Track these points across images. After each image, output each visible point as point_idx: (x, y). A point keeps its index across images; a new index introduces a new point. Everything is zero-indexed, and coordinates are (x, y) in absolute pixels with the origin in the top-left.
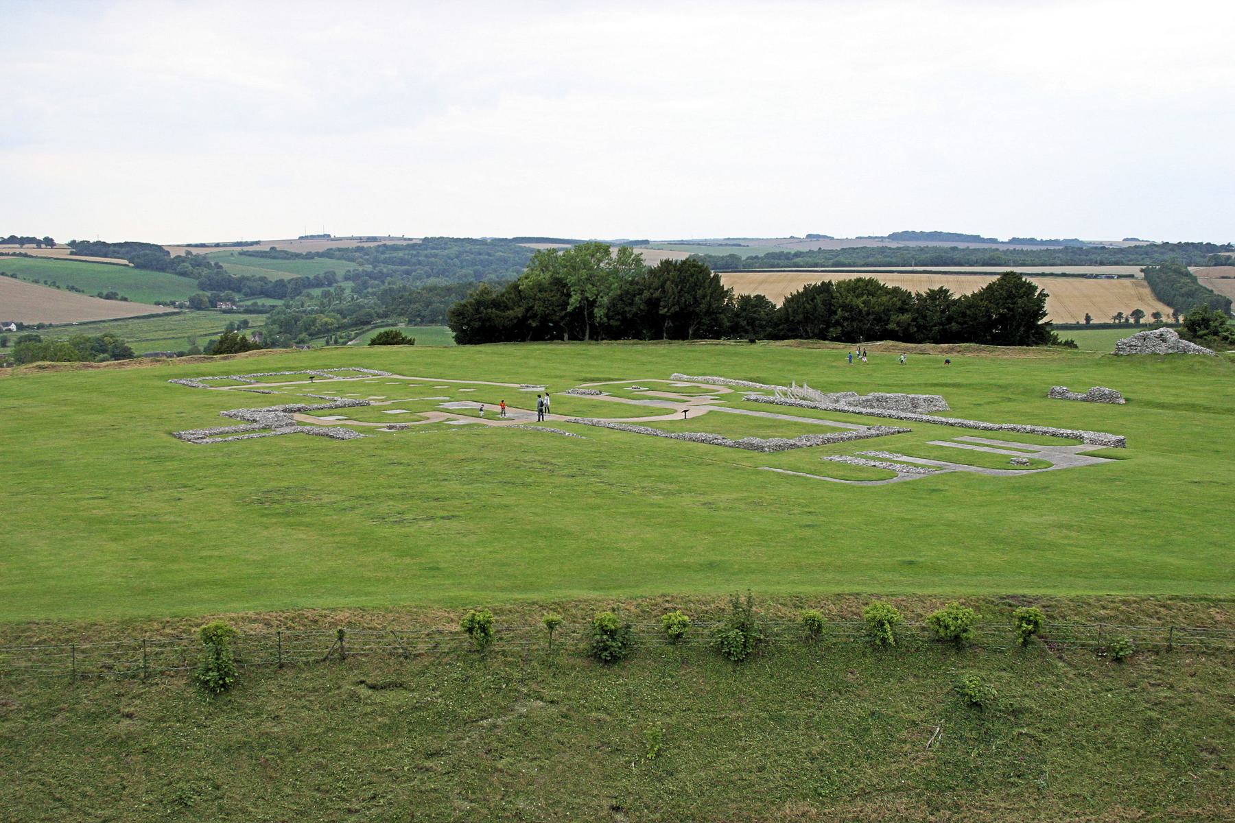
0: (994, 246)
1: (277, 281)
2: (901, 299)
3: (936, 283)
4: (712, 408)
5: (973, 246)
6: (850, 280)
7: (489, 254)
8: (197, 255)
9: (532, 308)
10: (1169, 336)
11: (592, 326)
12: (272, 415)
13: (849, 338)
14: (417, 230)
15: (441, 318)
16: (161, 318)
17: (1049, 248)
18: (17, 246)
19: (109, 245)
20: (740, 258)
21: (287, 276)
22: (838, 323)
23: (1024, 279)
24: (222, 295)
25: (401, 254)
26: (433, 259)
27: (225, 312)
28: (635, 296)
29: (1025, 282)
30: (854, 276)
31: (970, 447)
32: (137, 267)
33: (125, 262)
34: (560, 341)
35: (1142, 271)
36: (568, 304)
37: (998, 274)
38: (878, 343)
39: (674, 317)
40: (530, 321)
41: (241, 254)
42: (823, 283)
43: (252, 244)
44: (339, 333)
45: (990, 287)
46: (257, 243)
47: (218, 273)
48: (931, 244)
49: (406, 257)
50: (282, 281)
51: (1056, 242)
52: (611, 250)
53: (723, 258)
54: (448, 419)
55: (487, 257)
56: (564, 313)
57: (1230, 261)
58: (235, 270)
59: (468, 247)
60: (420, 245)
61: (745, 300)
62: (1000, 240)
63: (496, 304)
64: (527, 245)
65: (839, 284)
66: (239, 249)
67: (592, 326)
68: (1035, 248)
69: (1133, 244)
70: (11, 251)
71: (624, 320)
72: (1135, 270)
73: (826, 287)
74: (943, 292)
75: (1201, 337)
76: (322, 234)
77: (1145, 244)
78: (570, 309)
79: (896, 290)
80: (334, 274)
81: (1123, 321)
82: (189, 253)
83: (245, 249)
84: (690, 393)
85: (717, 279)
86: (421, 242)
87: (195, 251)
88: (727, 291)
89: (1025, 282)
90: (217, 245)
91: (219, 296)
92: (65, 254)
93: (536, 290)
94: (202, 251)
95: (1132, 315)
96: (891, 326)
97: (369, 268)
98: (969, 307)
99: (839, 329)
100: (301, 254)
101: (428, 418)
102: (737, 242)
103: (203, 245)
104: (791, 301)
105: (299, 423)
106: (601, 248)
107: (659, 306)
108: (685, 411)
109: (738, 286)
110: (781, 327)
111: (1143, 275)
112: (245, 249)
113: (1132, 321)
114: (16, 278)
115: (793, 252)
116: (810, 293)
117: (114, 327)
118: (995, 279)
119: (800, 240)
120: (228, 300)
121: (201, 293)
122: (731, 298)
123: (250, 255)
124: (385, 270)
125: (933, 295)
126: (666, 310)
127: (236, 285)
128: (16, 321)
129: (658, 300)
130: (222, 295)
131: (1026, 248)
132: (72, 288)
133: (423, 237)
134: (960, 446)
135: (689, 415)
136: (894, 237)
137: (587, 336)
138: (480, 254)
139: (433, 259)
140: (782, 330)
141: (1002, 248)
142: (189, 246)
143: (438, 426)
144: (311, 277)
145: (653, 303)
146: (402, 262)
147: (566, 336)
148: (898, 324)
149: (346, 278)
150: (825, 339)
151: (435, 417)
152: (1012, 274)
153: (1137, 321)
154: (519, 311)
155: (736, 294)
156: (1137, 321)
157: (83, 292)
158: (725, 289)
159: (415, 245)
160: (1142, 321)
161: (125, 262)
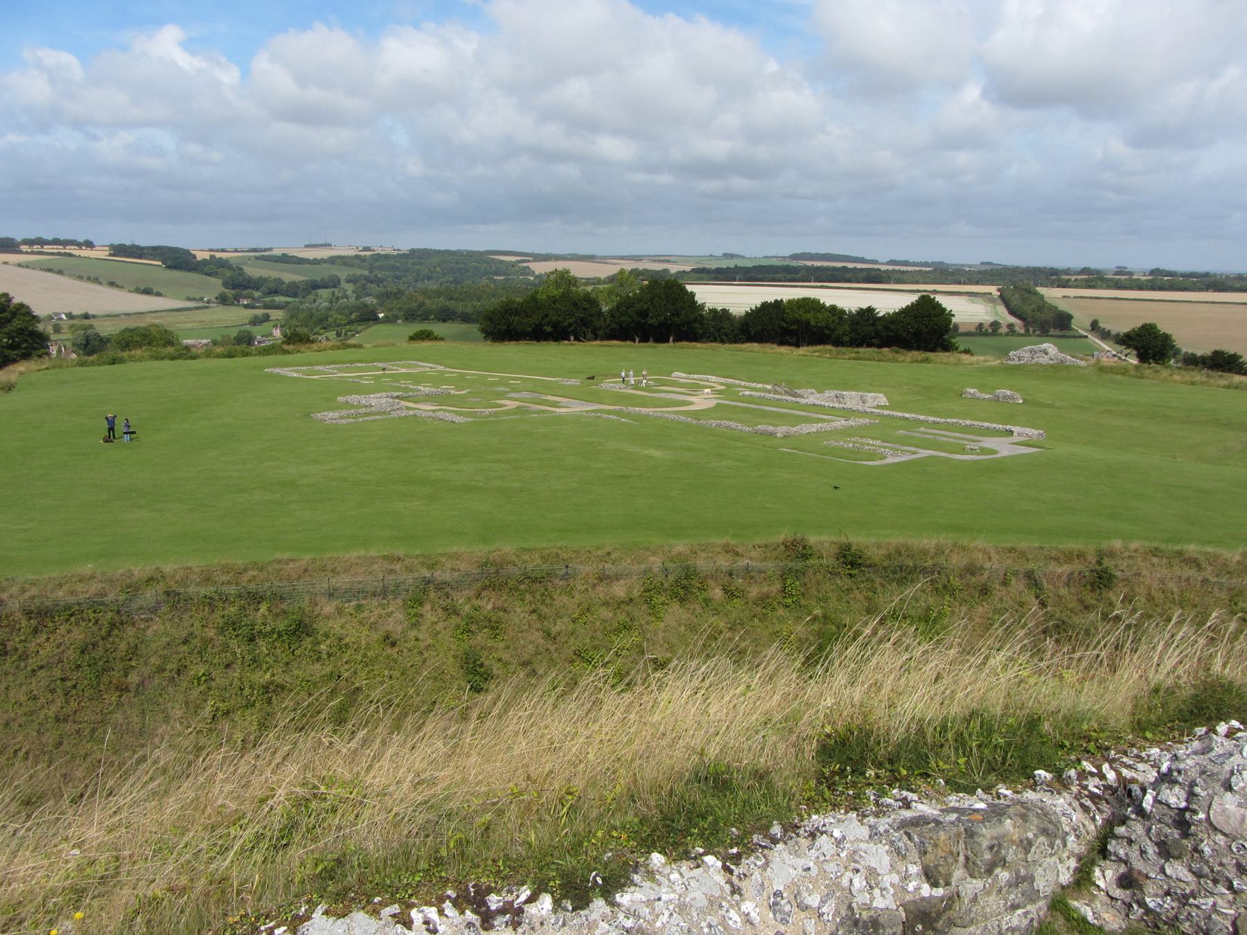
0: (876, 267)
1: (290, 283)
4: (719, 401)
5: (859, 266)
8: (221, 258)
9: (546, 315)
10: (1050, 350)
14: (422, 247)
16: (193, 312)
17: (922, 269)
18: (61, 247)
21: (298, 278)
24: (244, 293)
26: (418, 267)
27: (246, 307)
31: (956, 441)
32: (168, 267)
35: (998, 290)
40: (545, 327)
41: (257, 258)
43: (265, 250)
46: (270, 249)
47: (239, 275)
49: (397, 264)
50: (294, 282)
51: (926, 264)
53: (658, 272)
57: (1070, 283)
58: (253, 272)
60: (408, 255)
63: (516, 312)
64: (497, 257)
68: (910, 269)
69: (989, 268)
70: (56, 251)
72: (993, 290)
73: (778, 304)
74: (870, 310)
77: (1000, 267)
82: (212, 257)
84: (695, 388)
87: (218, 255)
91: (241, 294)
92: (102, 254)
94: (224, 255)
101: (505, 406)
102: (668, 258)
103: (223, 251)
109: (710, 296)
114: (62, 274)
117: (157, 318)
119: (718, 258)
120: (249, 297)
121: (226, 290)
123: (265, 260)
124: (379, 275)
125: (861, 312)
127: (255, 284)
128: (65, 312)
130: (244, 293)
132: (112, 284)
139: (418, 267)
141: (883, 268)
142: (211, 250)
144: (319, 279)
146: (394, 268)
147: (572, 338)
149: (348, 281)
157: (123, 287)
159: (404, 254)
161: (160, 263)
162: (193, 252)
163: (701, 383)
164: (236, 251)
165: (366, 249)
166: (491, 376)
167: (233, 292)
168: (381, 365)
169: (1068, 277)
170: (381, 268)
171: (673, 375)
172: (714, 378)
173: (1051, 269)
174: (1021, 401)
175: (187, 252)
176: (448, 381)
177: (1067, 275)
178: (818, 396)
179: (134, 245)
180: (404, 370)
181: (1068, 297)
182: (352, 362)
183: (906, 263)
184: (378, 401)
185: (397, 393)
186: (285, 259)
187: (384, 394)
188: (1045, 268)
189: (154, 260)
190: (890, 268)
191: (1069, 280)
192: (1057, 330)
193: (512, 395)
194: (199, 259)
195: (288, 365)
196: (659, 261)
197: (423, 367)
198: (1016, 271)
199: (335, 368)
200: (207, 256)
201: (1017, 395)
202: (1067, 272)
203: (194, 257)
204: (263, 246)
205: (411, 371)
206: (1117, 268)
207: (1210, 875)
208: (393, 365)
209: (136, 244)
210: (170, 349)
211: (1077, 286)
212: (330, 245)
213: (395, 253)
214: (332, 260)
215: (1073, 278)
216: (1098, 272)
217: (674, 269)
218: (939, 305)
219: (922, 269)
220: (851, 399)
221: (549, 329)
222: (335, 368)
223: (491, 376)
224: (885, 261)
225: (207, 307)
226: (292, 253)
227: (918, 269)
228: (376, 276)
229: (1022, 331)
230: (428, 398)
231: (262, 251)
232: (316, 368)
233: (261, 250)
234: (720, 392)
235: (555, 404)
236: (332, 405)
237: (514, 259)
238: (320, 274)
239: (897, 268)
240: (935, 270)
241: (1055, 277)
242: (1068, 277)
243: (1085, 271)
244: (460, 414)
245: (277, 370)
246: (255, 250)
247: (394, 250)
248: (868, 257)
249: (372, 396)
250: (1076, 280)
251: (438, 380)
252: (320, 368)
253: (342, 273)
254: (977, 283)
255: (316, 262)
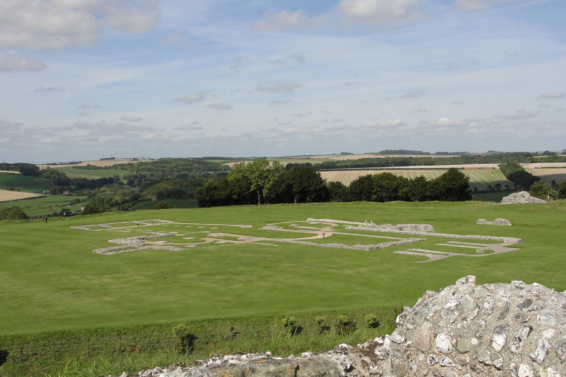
0: (429, 156)
2: (404, 182)
3: (418, 174)
5: (419, 156)
6: (380, 174)
7: (191, 166)
8: (52, 169)
11: (262, 198)
12: (134, 241)
13: (381, 200)
15: (172, 196)
17: (455, 156)
19: (10, 165)
20: (311, 164)
21: (97, 178)
22: (375, 193)
23: (459, 171)
25: (149, 166)
26: (164, 169)
28: (281, 183)
29: (460, 172)
30: (382, 172)
32: (24, 174)
33: (19, 173)
34: (247, 205)
35: (499, 166)
36: (251, 188)
37: (447, 169)
38: (394, 202)
39: (300, 193)
41: (73, 167)
42: (368, 175)
43: (78, 163)
44: (124, 205)
45: (444, 175)
46: (81, 162)
48: (400, 156)
49: (152, 168)
50: (94, 180)
51: (457, 154)
52: (269, 162)
54: (215, 241)
55: (190, 167)
56: (248, 192)
58: (72, 176)
59: (181, 162)
60: (158, 162)
61: (332, 184)
62: (431, 153)
64: (209, 161)
65: (375, 175)
66: (72, 165)
67: (262, 198)
68: (448, 156)
71: (277, 195)
72: (496, 165)
73: (369, 177)
74: (422, 178)
75: (539, 195)
76: (111, 157)
78: (251, 190)
79: (401, 178)
80: (118, 176)
81: (491, 189)
82: (49, 168)
83: (75, 165)
84: (320, 226)
85: (319, 175)
86: (159, 160)
87: (51, 167)
88: (324, 180)
89: (460, 172)
90: (62, 164)
93: (235, 181)
95: (496, 186)
96: (400, 194)
97: (135, 173)
98: (435, 184)
99: (376, 196)
100: (102, 167)
101: (206, 241)
103: (55, 164)
104: (354, 184)
105: (148, 245)
106: (264, 161)
107: (293, 188)
108: (324, 234)
109: (329, 177)
110: (349, 196)
111: (499, 167)
112: (75, 165)
113: (496, 189)
115: (336, 161)
116: (362, 180)
118: (446, 171)
122: (326, 183)
126: (296, 189)
129: (292, 184)
131: (444, 156)
133: (159, 158)
134: (451, 245)
135: (325, 236)
136: (382, 153)
137: (259, 203)
138: (187, 166)
140: (350, 197)
141: (433, 157)
142: (48, 164)
143: (212, 244)
145: (290, 186)
146: (150, 170)
148: (403, 193)
150: (369, 201)
151: (209, 240)
152: (454, 169)
153: (498, 189)
154: (227, 192)
155: (328, 181)
156: (498, 189)
158: (323, 179)
159: (156, 162)
160: (500, 189)
162: (37, 166)
163: (323, 223)
164: (62, 164)
165: (135, 159)
166: (200, 226)
167: (60, 187)
168: (137, 222)
169: (536, 157)
170: (143, 170)
171: (307, 220)
172: (330, 221)
173: (527, 153)
174: (510, 225)
175: (34, 166)
176: (176, 229)
177: (536, 156)
178: (393, 227)
179: (5, 163)
180: (149, 225)
181: (538, 168)
182: (120, 221)
183: (446, 154)
184: (133, 242)
185: (143, 237)
186: (89, 167)
187: (136, 238)
188: (524, 152)
189: (16, 171)
190: (437, 156)
191: (537, 159)
192: (398, 175)
193: (211, 235)
194: (40, 170)
195: (84, 224)
196: (304, 159)
197: (162, 222)
198: (509, 155)
199: (109, 225)
200: (45, 167)
201: (508, 221)
202: (536, 154)
203: (38, 168)
204: (76, 161)
205: (154, 225)
206: (564, 150)
207: (76, 351)
208: (144, 222)
209: (6, 163)
210: (337, 266)
211: (542, 161)
212: (114, 158)
213: (151, 161)
214: (115, 167)
215: (540, 157)
216: (553, 154)
217: (313, 163)
218: (462, 173)
219: (455, 156)
220: (408, 229)
221: (235, 197)
222: (109, 225)
223: (200, 226)
224: (434, 153)
225: (45, 196)
226: (92, 164)
227: (453, 156)
228: (140, 174)
229: (514, 188)
230: (161, 238)
231: (66, 164)
232: (100, 225)
233: (76, 163)
234: (335, 228)
235: (235, 239)
236: (104, 244)
237: (219, 161)
238: (107, 175)
239: (441, 156)
240: (463, 157)
241: (530, 157)
242: (536, 157)
243: (547, 153)
244: (177, 246)
245: (77, 227)
246: (72, 163)
247: (151, 159)
248: (424, 151)
249: (128, 239)
250: (541, 158)
251: (171, 227)
252: (102, 225)
253: (122, 174)
254: (486, 163)
255: (107, 168)
